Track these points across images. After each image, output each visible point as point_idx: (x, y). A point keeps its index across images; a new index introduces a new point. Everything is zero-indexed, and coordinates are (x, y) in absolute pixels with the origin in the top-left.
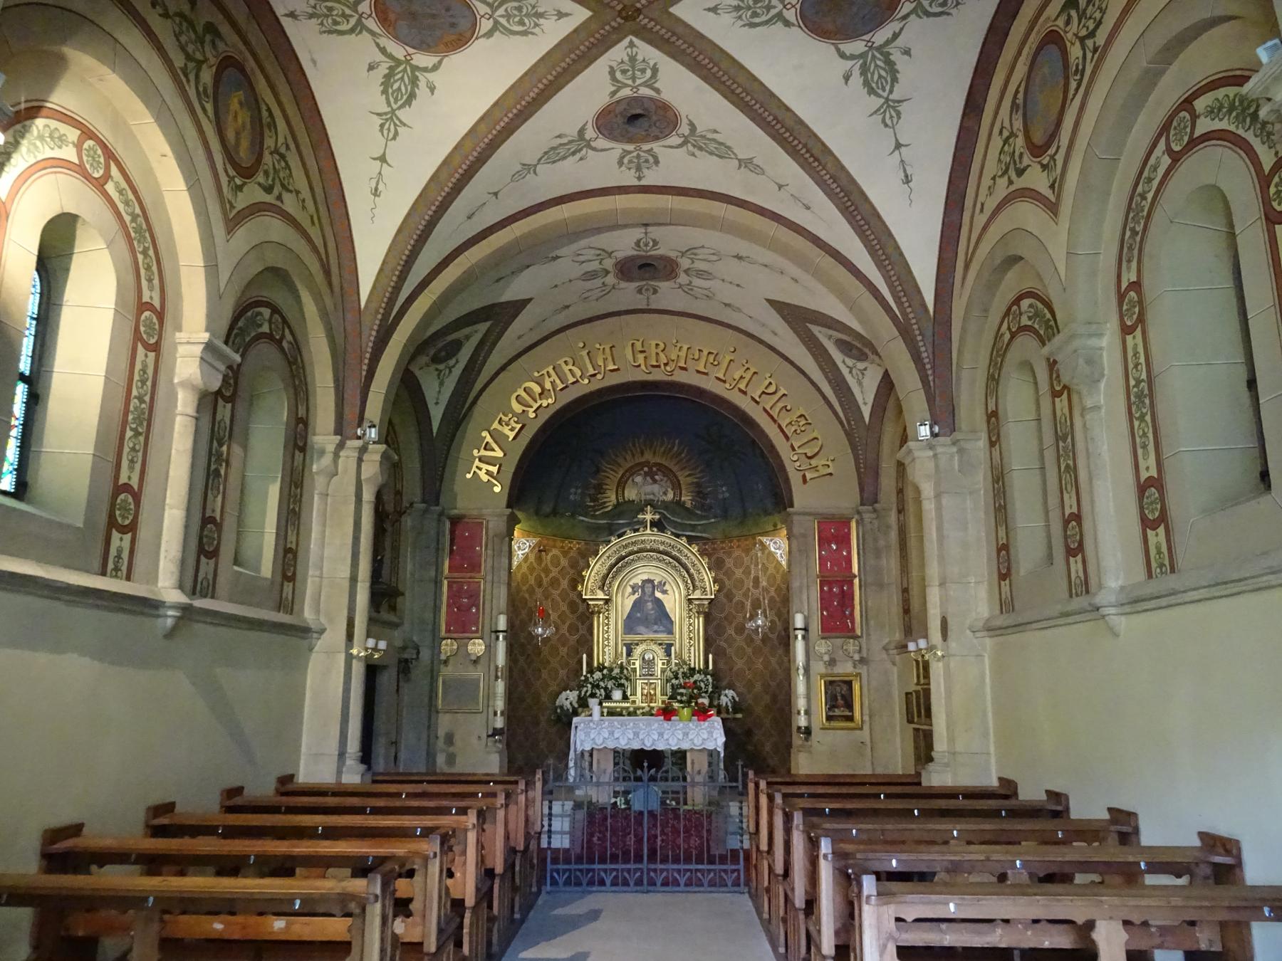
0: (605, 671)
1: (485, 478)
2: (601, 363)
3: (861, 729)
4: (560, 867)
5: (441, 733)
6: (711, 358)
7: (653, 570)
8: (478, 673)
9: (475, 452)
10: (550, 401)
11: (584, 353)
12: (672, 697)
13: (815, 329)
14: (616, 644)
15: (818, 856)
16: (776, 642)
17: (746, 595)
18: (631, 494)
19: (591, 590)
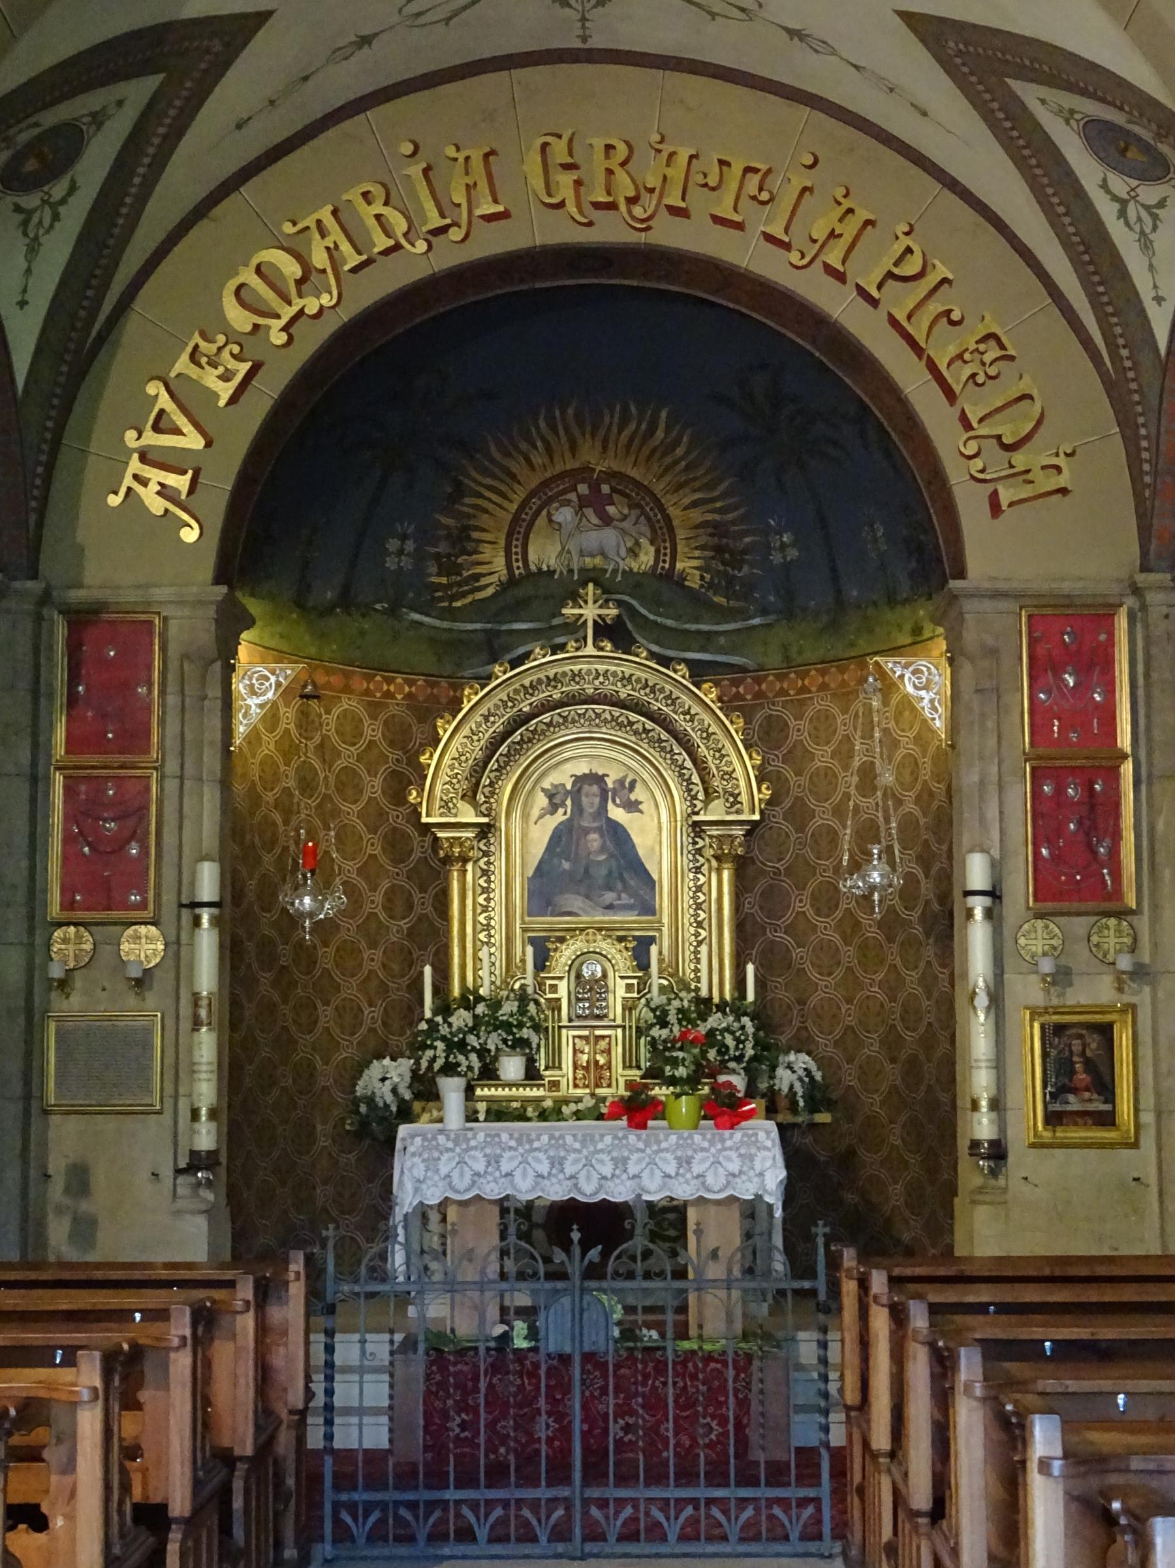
0: (480, 1009)
1: (157, 505)
2: (459, 197)
3: (1135, 1145)
4: (360, 1496)
5: (57, 1165)
6: (753, 181)
7: (604, 751)
8: (151, 1011)
9: (130, 436)
10: (325, 300)
11: (415, 170)
12: (654, 1073)
13: (1030, 94)
14: (509, 940)
15: (1023, 1463)
16: (918, 931)
17: (839, 812)
18: (544, 553)
19: (442, 803)
